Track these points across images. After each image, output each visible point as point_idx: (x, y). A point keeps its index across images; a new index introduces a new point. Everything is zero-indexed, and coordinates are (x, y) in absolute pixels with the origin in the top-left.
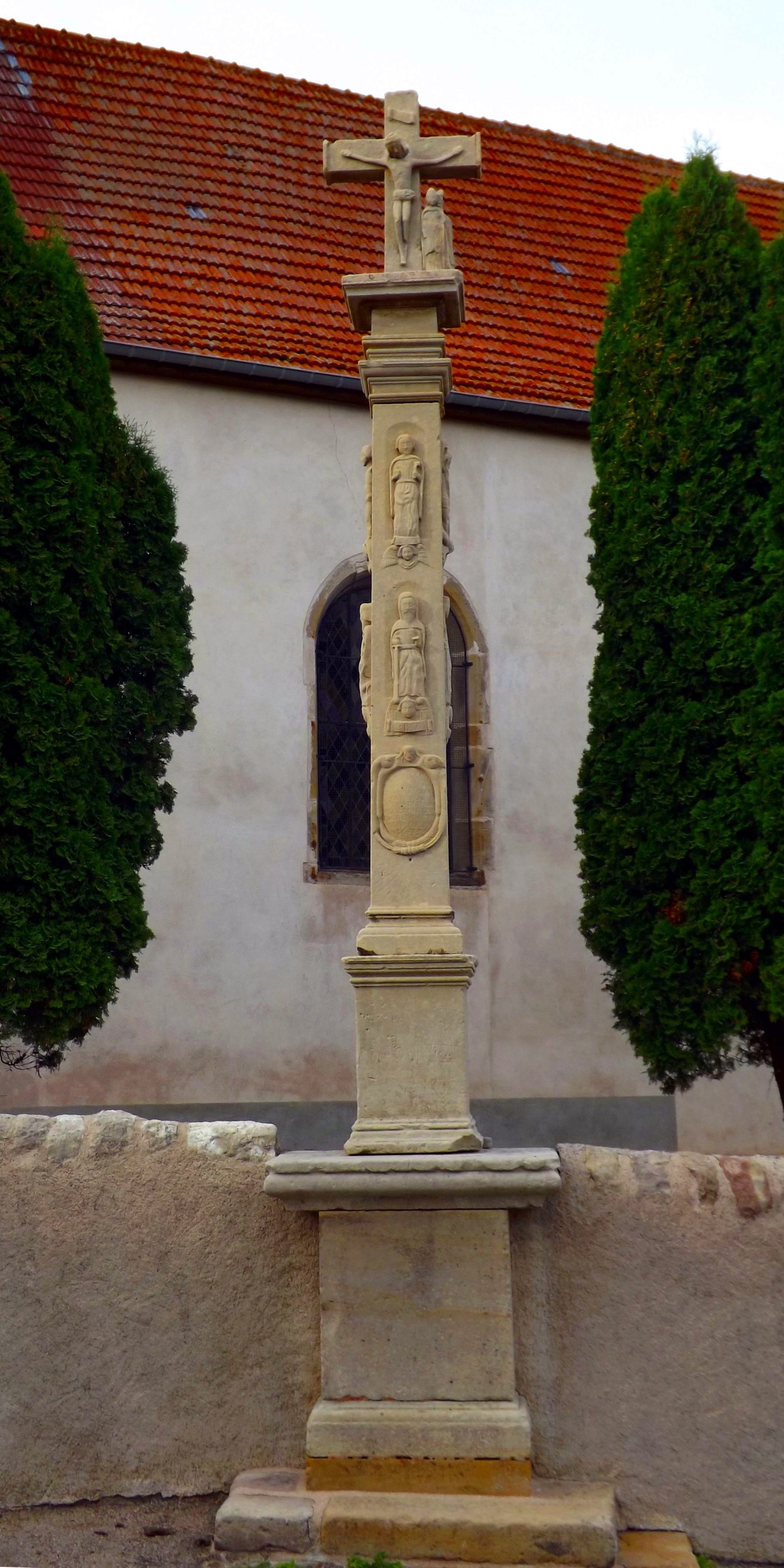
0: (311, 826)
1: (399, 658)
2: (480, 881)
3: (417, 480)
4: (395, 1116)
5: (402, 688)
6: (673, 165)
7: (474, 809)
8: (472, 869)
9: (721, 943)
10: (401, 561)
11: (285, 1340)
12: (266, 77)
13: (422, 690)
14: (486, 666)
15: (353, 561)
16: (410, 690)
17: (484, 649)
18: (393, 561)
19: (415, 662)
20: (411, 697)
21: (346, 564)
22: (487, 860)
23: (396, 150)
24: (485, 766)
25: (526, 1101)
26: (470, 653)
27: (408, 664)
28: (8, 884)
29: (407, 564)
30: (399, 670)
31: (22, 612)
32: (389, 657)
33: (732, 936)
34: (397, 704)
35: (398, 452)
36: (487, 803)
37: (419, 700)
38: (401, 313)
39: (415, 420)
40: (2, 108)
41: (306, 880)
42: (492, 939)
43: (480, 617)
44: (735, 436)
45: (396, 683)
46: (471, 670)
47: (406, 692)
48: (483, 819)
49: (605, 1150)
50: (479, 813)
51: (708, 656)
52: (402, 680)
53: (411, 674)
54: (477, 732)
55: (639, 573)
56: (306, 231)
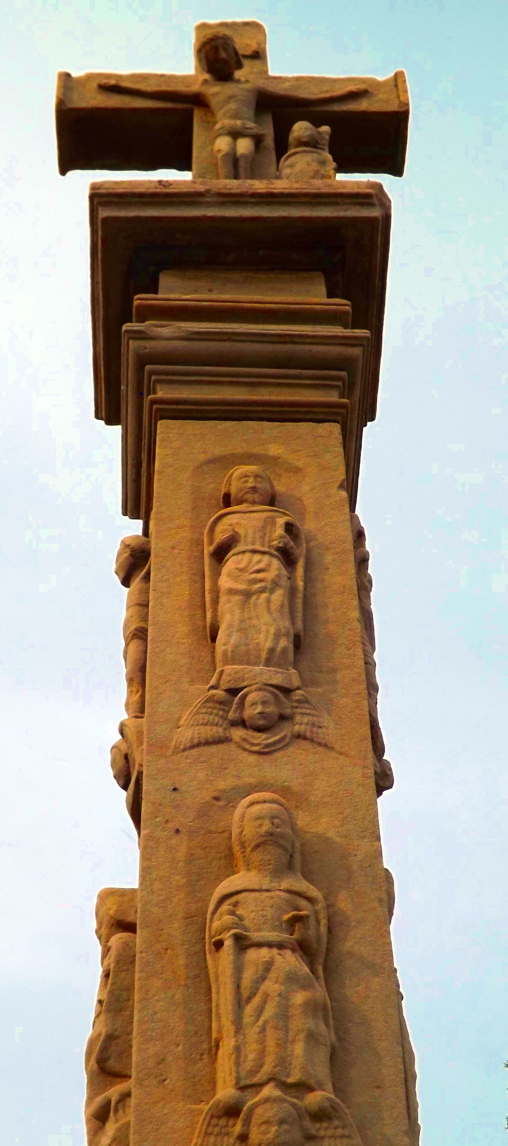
1: (238, 970)
3: (287, 557)
4: (205, 934)
5: (251, 1056)
6: (381, 862)
10: (238, 733)
13: (321, 1070)
16: (283, 1062)
18: (219, 731)
19: (292, 979)
20: (284, 1086)
23: (223, 55)
27: (270, 986)
30: (240, 1002)
32: (201, 981)
34: (232, 1111)
37: (314, 1099)
38: (236, 276)
39: (274, 450)
40: (207, 1145)
45: (228, 1045)
47: (268, 1068)
52: (252, 1033)
53: (284, 1014)
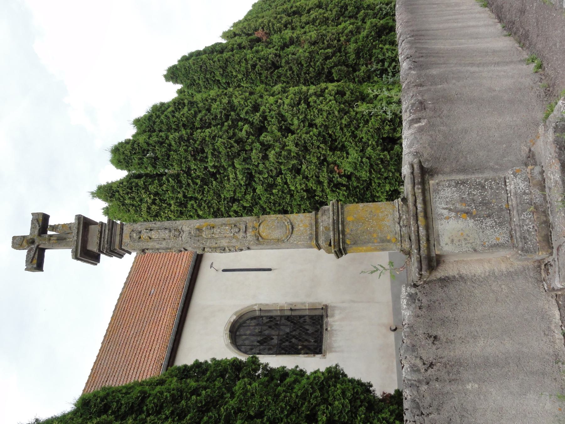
0: (309, 357)
2: (326, 306)
7: (304, 308)
8: (322, 309)
9: (334, 177)
11: (489, 275)
12: (88, 381)
14: (261, 304)
15: (226, 343)
17: (256, 305)
21: (227, 345)
22: (320, 304)
24: (291, 304)
25: (392, 293)
26: (257, 309)
28: (312, 417)
29: (182, 233)
31: (203, 410)
33: (331, 174)
35: (140, 238)
36: (303, 304)
41: (325, 358)
42: (343, 302)
43: (246, 306)
44: (174, 180)
46: (262, 309)
48: (307, 305)
49: (404, 405)
50: (305, 306)
51: (241, 185)
54: (281, 307)
55: (215, 209)
56: (130, 364)
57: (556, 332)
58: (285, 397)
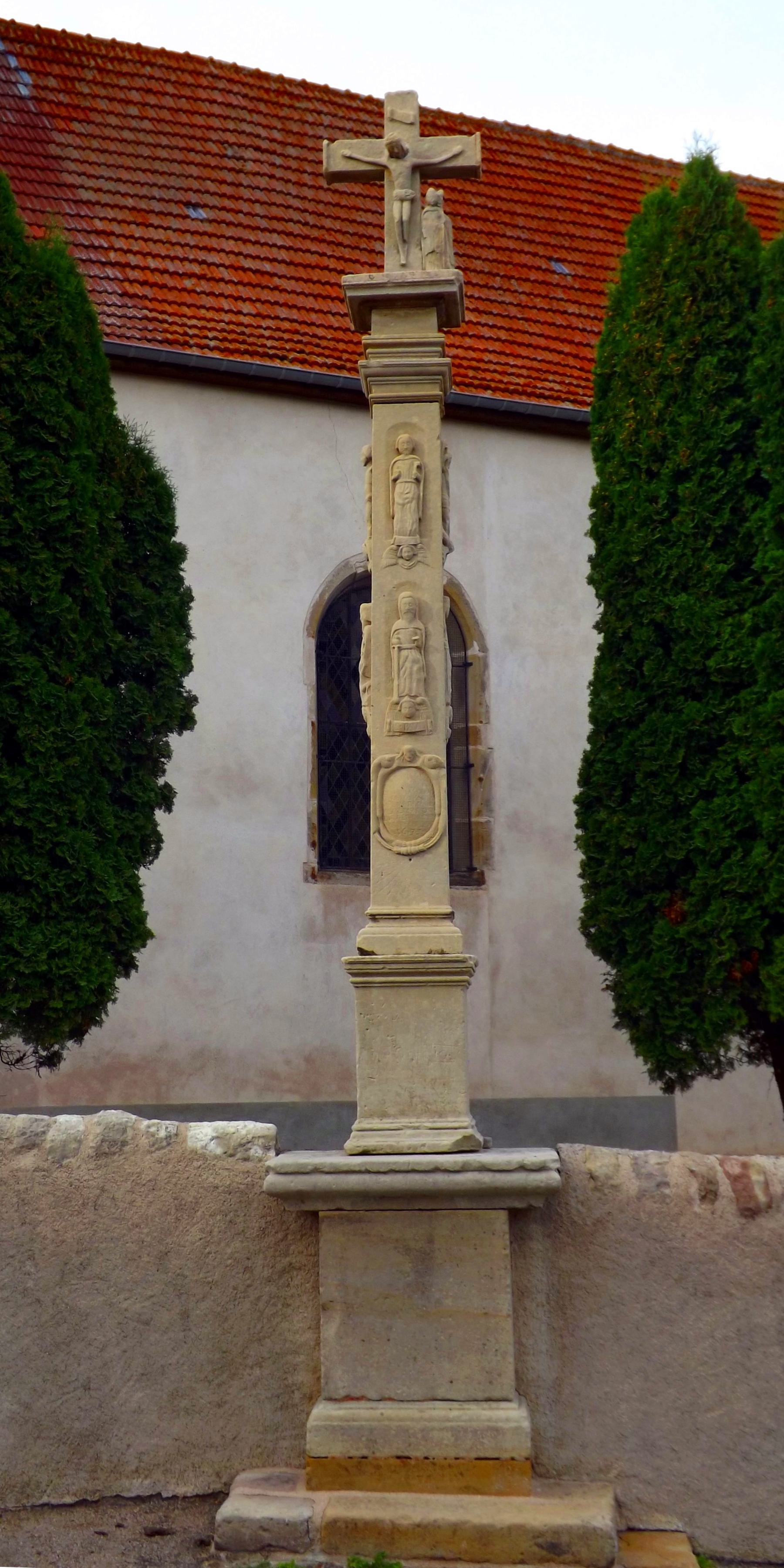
0: (311, 826)
1: (399, 658)
2: (480, 881)
3: (417, 480)
4: (395, 1116)
5: (402, 688)
6: (673, 165)
7: (474, 809)
8: (472, 869)
9: (721, 943)
10: (401, 561)
11: (285, 1340)
12: (266, 77)
13: (422, 690)
14: (486, 666)
15: (353, 561)
16: (410, 690)
17: (484, 649)
18: (393, 561)
19: (415, 662)
20: (411, 697)
21: (346, 564)
22: (487, 860)
23: (396, 150)
24: (485, 766)
25: (526, 1101)
26: (470, 653)
27: (408, 664)
28: (8, 884)
29: (407, 564)
30: (399, 670)
31: (22, 612)
32: (389, 657)
33: (732, 936)
34: (397, 704)
35: (398, 452)
36: (487, 803)
37: (419, 700)
38: (401, 313)
39: (415, 420)
40: (2, 108)
41: (306, 880)
42: (492, 939)
43: (480, 617)
44: (735, 436)
45: (396, 683)
46: (471, 670)
47: (406, 692)
48: (483, 819)
50: (479, 813)
51: (708, 656)
52: (402, 680)
53: (411, 674)
54: (477, 732)
55: (639, 573)
56: (306, 231)
57: (147, 1482)
58: (58, 819)
